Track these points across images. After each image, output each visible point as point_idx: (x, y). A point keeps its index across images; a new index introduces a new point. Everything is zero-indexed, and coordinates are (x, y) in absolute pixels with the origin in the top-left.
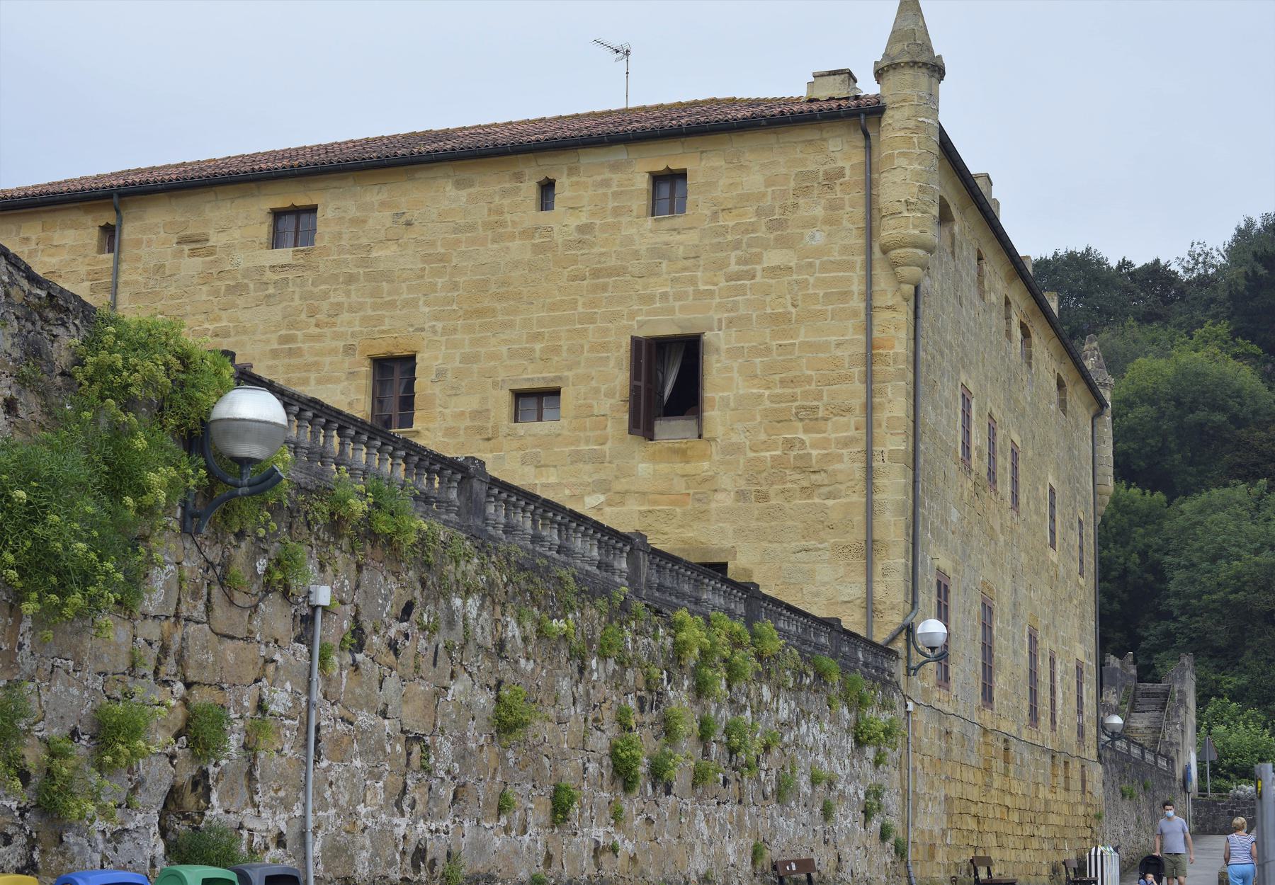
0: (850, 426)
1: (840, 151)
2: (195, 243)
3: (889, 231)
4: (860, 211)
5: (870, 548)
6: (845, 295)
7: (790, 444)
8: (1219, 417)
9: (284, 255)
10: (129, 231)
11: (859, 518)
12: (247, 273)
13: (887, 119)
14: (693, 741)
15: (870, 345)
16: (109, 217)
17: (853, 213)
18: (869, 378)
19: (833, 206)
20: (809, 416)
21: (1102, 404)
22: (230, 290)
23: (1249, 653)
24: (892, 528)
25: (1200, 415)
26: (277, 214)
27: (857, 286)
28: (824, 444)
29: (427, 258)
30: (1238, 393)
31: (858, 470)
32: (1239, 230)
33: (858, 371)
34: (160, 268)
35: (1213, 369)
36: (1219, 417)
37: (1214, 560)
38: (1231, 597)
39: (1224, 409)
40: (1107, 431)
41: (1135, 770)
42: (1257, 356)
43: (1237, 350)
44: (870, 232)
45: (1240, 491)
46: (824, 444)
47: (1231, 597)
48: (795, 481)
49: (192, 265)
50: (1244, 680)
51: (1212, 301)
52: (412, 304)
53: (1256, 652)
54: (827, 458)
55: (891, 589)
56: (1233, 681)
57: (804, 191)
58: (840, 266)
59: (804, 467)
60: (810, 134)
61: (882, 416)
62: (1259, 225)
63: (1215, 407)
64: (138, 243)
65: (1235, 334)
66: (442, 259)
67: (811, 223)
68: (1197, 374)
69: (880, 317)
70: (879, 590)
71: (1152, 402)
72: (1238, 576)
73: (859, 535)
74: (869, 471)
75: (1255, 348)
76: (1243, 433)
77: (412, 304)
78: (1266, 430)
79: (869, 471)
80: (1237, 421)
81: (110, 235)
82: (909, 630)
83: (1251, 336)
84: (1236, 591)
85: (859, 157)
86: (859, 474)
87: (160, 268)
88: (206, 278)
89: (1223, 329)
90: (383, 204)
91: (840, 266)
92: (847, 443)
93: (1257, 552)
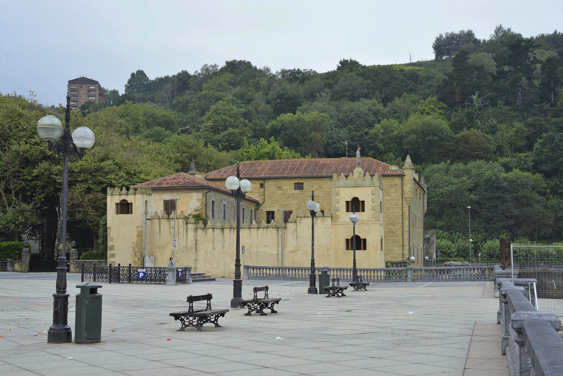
0: (399, 226)
1: (398, 181)
2: (280, 188)
3: (405, 196)
4: (401, 191)
5: (403, 245)
6: (398, 205)
7: (390, 229)
8: (436, 138)
9: (298, 191)
10: (266, 185)
11: (401, 241)
12: (290, 194)
13: (405, 177)
14: (192, 232)
15: (403, 213)
16: (262, 182)
17: (400, 192)
18: (403, 218)
19: (396, 190)
20: (393, 225)
21: (425, 192)
22: (288, 197)
23: (445, 215)
24: (406, 242)
25: (430, 138)
26: (295, 183)
27: (400, 203)
28: (395, 229)
29: (325, 194)
30: (441, 130)
31: (401, 233)
32: (437, 38)
33: (401, 217)
34: (273, 192)
35: (434, 122)
36: (436, 138)
37: (435, 188)
38: (440, 199)
39: (437, 135)
40: (426, 197)
41: (519, 337)
42: (445, 108)
43: (439, 106)
44: (402, 195)
45: (442, 165)
46: (395, 229)
47: (440, 199)
48: (391, 234)
49: (279, 192)
50: (443, 223)
51: (431, 86)
52: (323, 202)
53: (447, 215)
54: (396, 231)
55: (406, 252)
56: (440, 224)
57: (392, 187)
58: (397, 200)
59: (392, 232)
60: (392, 178)
61: (405, 225)
62: (444, 37)
63: (435, 134)
64: (268, 187)
65: (439, 100)
66: (328, 194)
67: (393, 192)
68: (429, 125)
69: (404, 209)
70: (404, 252)
71: (416, 133)
72: (442, 193)
73: (401, 243)
74: (403, 233)
75: (445, 105)
76: (443, 143)
77: (323, 202)
78: (449, 142)
79: (403, 233)
80: (441, 139)
81: (262, 185)
82: (409, 258)
83: (443, 101)
84: (441, 198)
85: (400, 182)
86: (401, 234)
87: (273, 192)
88: (282, 195)
89: (435, 98)
90: (316, 184)
91: (397, 200)
92: (399, 229)
93: (447, 186)
